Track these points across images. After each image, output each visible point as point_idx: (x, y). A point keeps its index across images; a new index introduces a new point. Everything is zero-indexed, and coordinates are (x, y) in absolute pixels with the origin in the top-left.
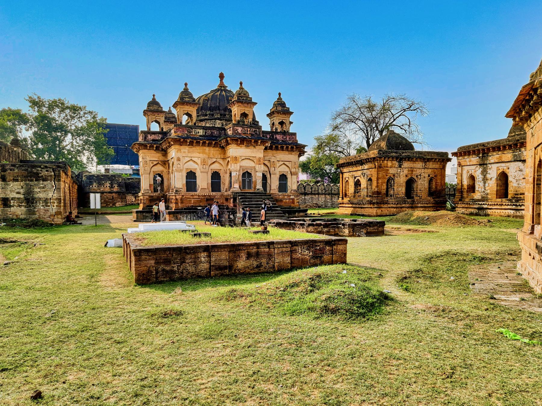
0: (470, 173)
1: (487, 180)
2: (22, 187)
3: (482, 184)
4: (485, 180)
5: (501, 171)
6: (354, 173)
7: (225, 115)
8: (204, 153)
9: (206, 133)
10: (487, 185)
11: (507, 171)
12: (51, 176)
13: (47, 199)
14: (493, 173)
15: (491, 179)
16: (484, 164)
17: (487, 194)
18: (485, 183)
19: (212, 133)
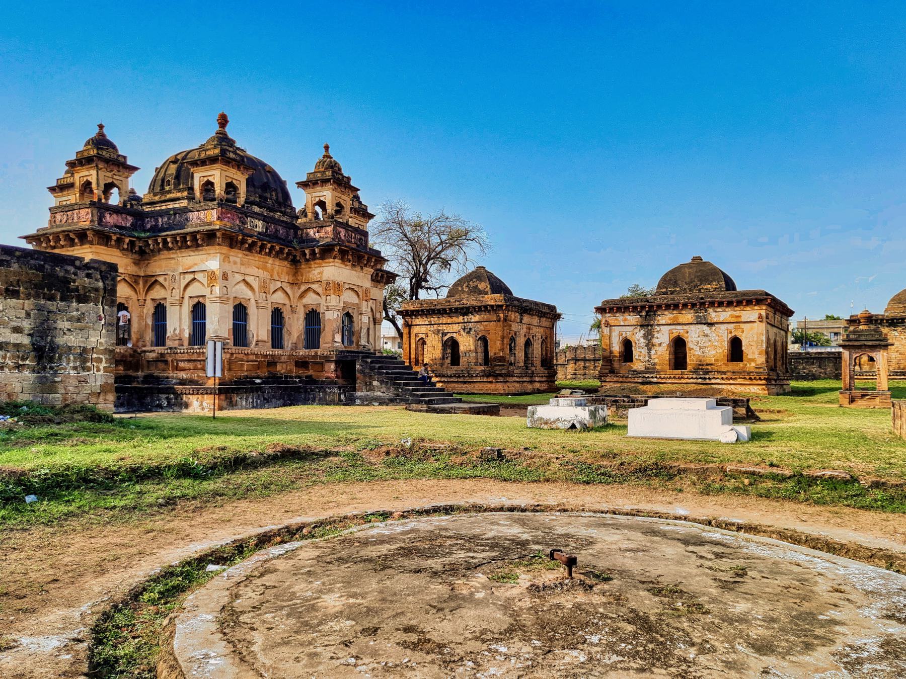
0: (624, 335)
1: (653, 345)
2: (28, 315)
3: (644, 351)
4: (650, 346)
5: (675, 335)
6: (444, 327)
7: (266, 199)
8: (264, 268)
9: (267, 229)
10: (653, 352)
11: (684, 336)
12: (97, 290)
13: (85, 350)
14: (663, 337)
15: (660, 345)
16: (648, 325)
17: (655, 364)
18: (649, 350)
19: (277, 231)
